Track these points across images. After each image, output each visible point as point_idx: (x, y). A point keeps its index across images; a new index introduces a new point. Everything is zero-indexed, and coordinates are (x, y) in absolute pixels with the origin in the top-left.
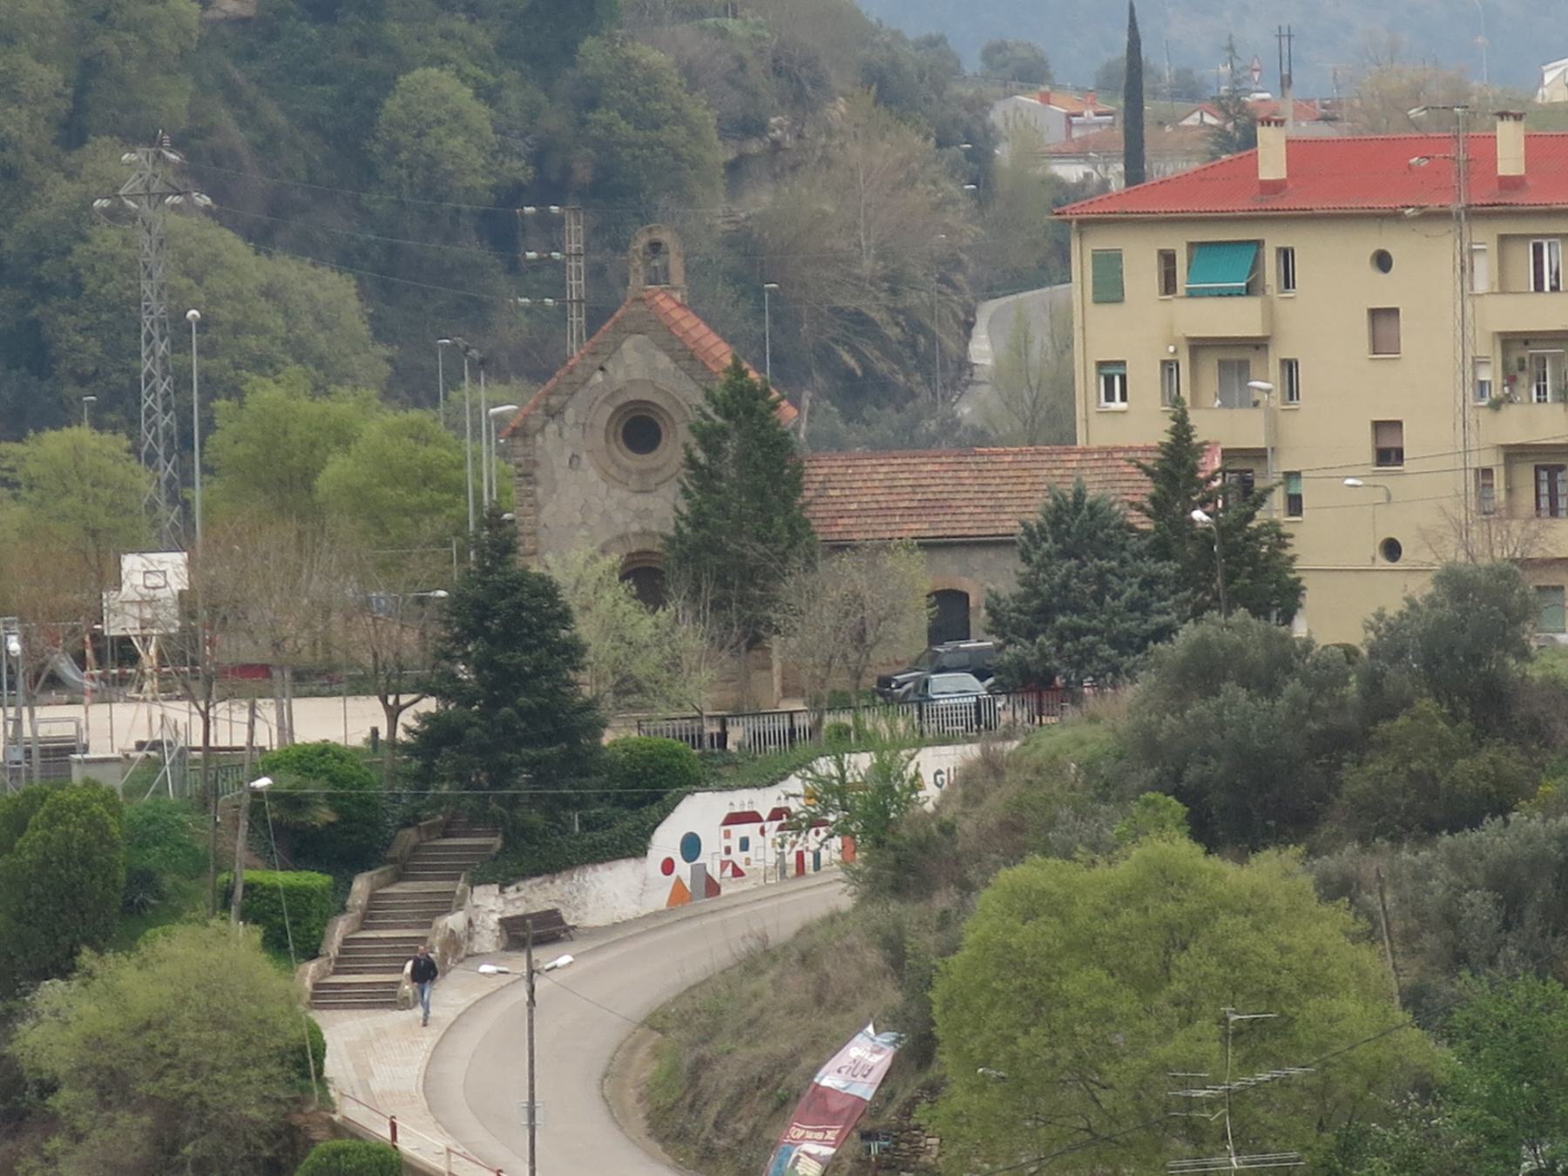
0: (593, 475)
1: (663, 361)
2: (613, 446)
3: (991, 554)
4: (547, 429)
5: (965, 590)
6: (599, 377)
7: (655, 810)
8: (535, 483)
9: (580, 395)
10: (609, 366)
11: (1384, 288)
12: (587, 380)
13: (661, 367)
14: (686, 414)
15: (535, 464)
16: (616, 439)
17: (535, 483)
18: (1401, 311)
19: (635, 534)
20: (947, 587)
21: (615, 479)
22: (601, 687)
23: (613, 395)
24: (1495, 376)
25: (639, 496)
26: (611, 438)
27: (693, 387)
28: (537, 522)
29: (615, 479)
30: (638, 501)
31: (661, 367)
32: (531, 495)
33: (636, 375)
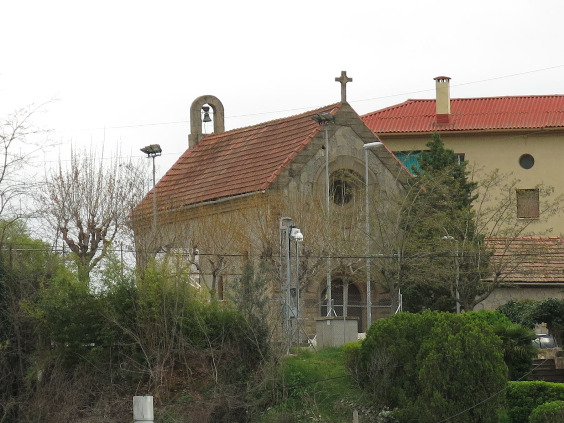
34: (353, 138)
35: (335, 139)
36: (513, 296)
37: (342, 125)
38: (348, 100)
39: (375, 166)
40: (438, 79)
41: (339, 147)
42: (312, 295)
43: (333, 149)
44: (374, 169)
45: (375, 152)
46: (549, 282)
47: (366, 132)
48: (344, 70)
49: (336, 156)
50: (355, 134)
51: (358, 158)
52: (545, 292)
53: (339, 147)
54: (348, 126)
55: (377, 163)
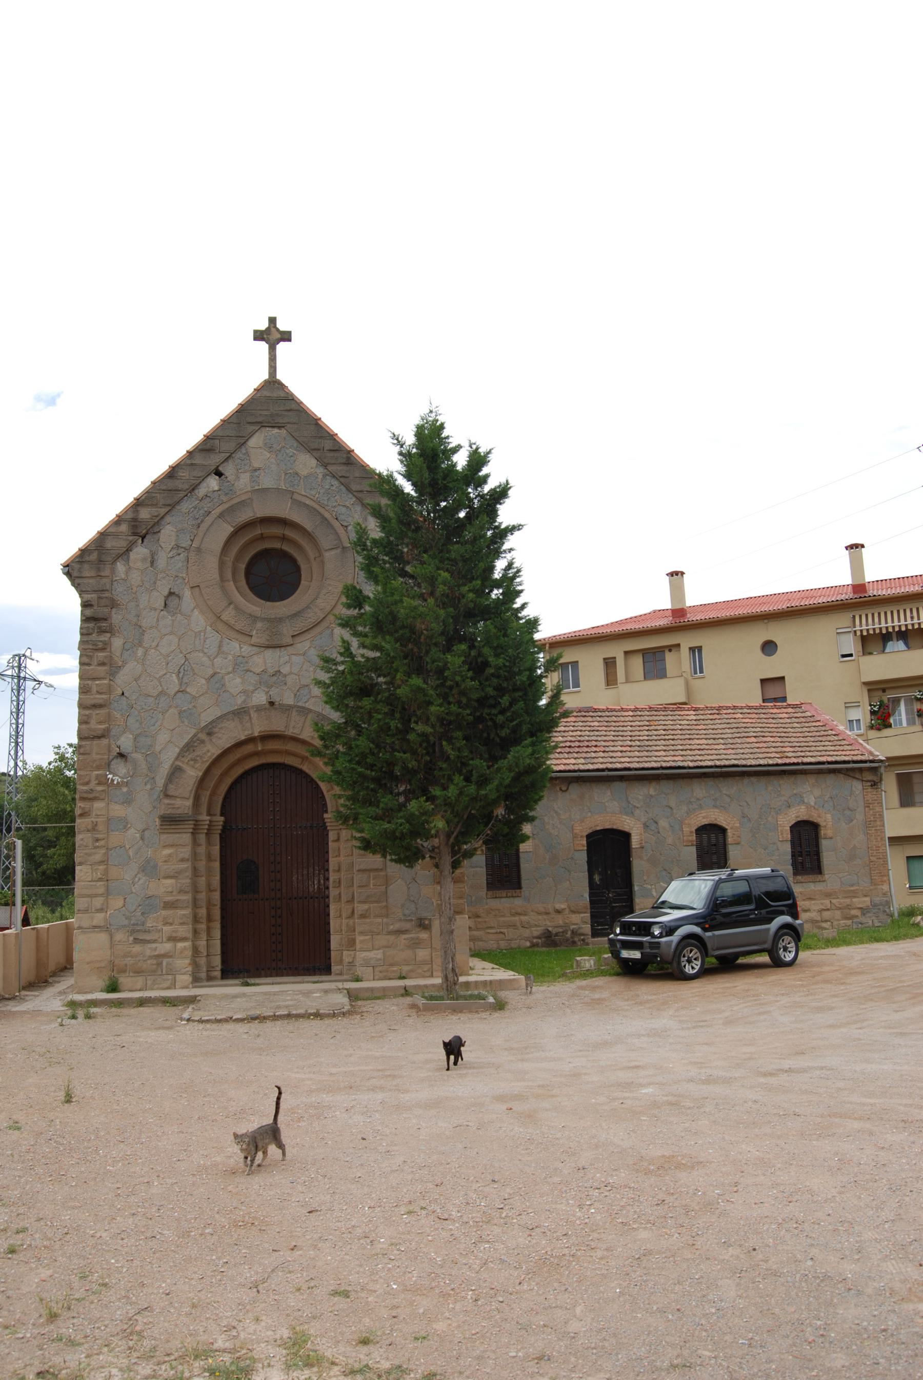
0: (199, 620)
1: (307, 464)
2: (231, 586)
3: (651, 789)
4: (133, 555)
5: (626, 828)
6: (213, 483)
7: (200, 447)
8: (110, 631)
9: (185, 506)
10: (228, 470)
11: (771, 667)
12: (194, 488)
13: (304, 472)
14: (338, 538)
15: (113, 604)
16: (235, 580)
17: (110, 631)
18: (786, 679)
19: (259, 709)
20: (608, 827)
21: (231, 627)
22: (897, 1279)
23: (231, 510)
24: (864, 714)
25: (269, 653)
26: (229, 575)
27: (350, 500)
28: (110, 690)
29: (231, 627)
30: (268, 660)
31: (304, 472)
32: (103, 649)
33: (267, 482)
34: (291, 451)
35: (247, 454)
36: (724, 792)
37: (262, 425)
38: (279, 376)
39: (344, 510)
40: (672, 574)
41: (256, 470)
42: (178, 802)
43: (242, 476)
44: (342, 517)
45: (341, 479)
46: (785, 764)
47: (321, 437)
48: (273, 315)
49: (249, 489)
50: (295, 444)
51: (303, 493)
52: (781, 782)
53: (256, 470)
54: (279, 427)
55: (347, 504)
